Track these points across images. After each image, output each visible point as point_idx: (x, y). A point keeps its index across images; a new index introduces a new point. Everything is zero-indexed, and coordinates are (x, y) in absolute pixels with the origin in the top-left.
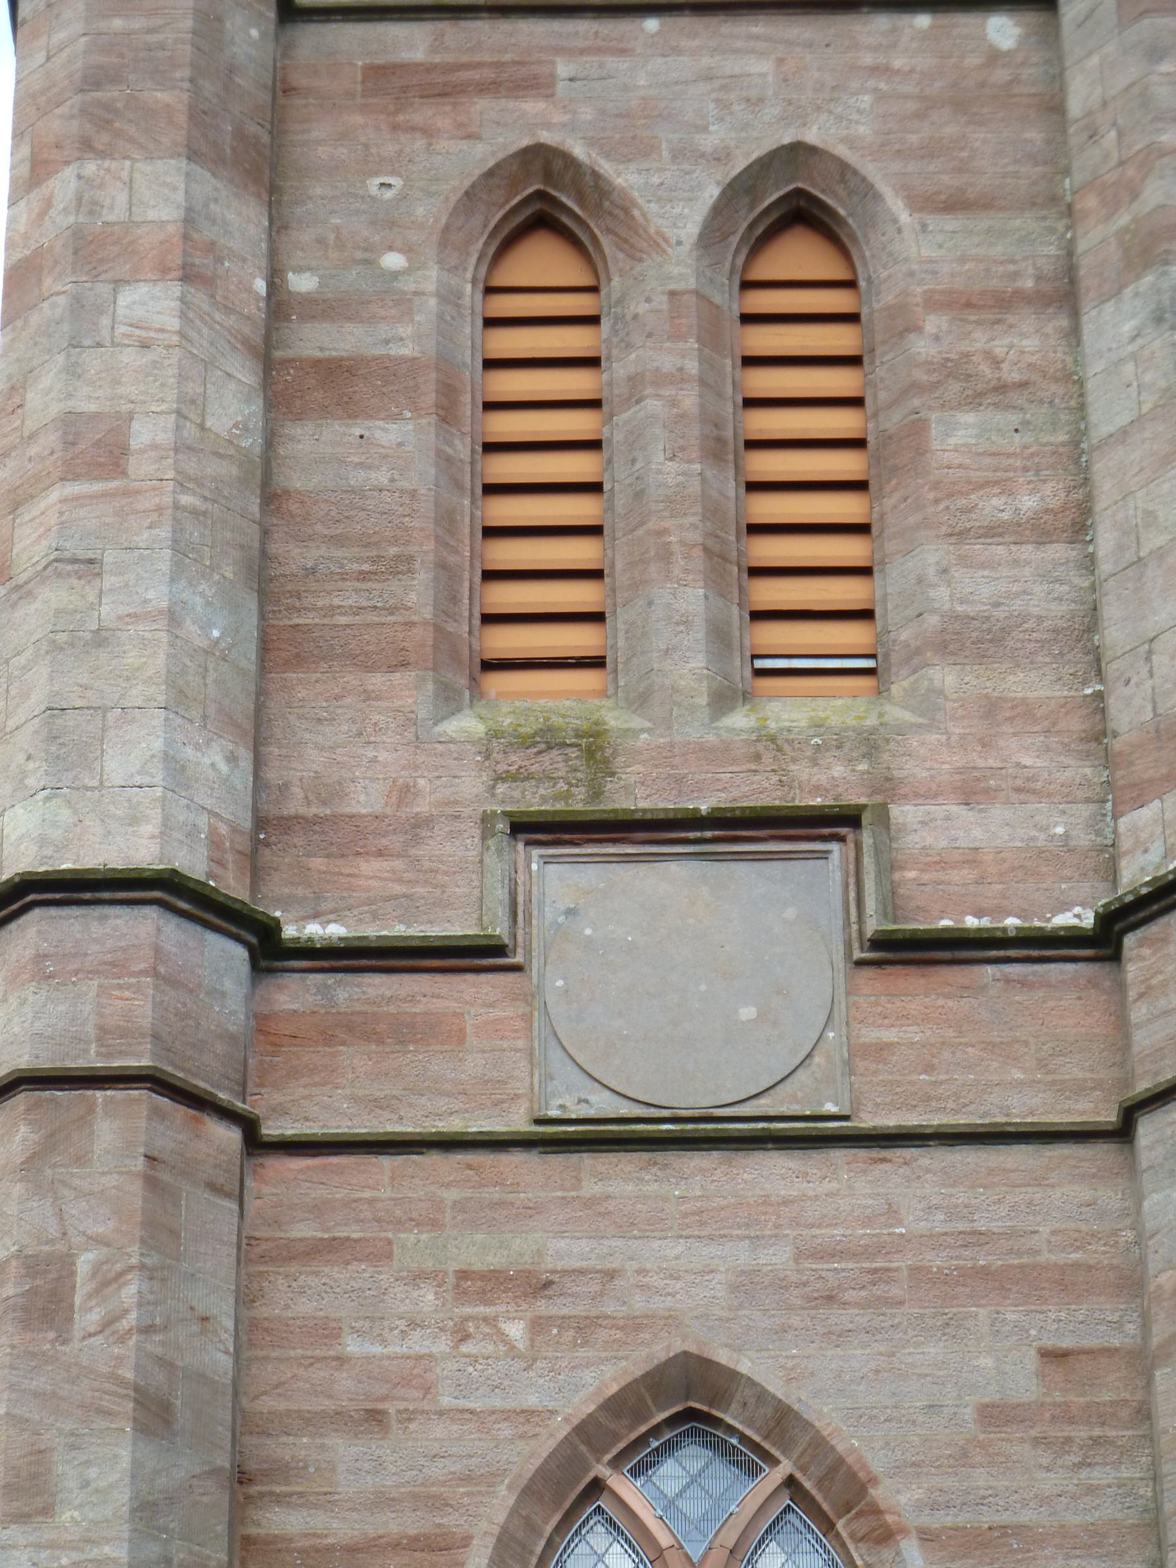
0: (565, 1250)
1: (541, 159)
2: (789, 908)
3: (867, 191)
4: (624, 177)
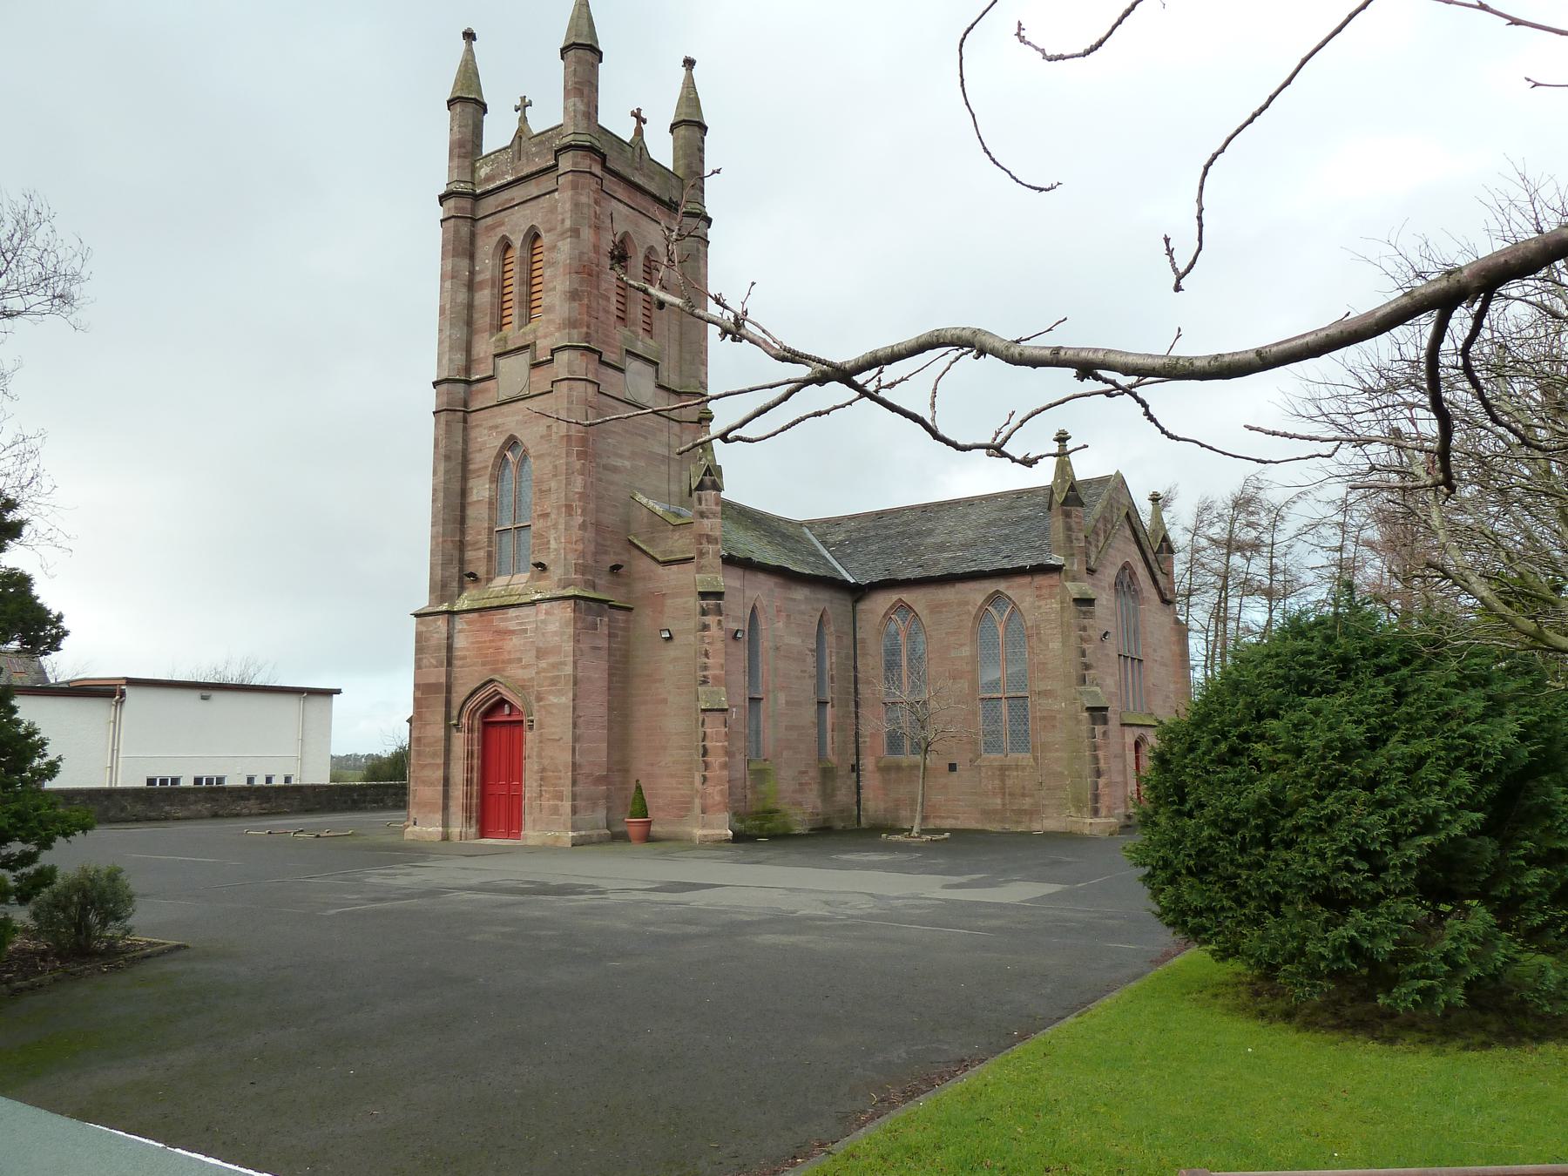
0: (500, 421)
2: (524, 359)
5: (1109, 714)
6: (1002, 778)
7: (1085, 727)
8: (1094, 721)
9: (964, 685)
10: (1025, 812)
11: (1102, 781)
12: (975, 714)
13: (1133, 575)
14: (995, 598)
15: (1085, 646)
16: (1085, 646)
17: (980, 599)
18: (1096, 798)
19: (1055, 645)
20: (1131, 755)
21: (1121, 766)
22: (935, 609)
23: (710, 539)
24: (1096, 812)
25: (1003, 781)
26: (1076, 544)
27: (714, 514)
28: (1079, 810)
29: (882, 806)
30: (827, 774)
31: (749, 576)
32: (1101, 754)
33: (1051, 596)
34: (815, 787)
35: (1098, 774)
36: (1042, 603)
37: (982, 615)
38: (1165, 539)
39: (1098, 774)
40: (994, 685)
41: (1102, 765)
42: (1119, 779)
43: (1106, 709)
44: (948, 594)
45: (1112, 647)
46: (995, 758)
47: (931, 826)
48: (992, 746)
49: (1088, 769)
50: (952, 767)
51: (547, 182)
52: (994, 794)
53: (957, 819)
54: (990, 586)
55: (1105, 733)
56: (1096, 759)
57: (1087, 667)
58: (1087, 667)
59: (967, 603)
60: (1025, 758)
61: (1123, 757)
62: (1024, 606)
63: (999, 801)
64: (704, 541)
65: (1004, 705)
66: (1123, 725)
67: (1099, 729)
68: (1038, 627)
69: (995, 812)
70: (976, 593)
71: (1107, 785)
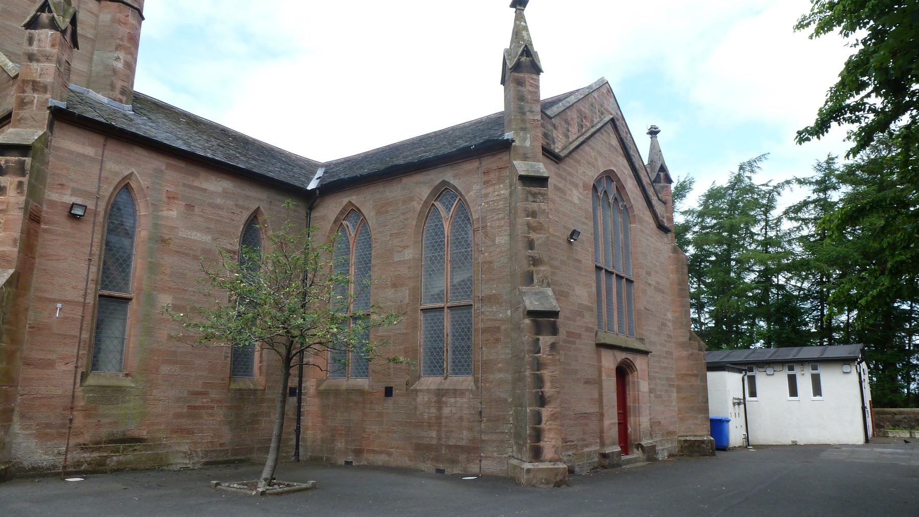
5: (560, 320)
6: (440, 405)
7: (527, 338)
8: (538, 329)
9: (404, 294)
10: (463, 449)
11: (546, 412)
12: (415, 327)
13: (621, 188)
14: (443, 191)
15: (533, 235)
16: (533, 235)
17: (425, 192)
18: (538, 435)
19: (502, 239)
20: (610, 384)
21: (596, 395)
22: (381, 210)
23: (36, 86)
24: (537, 454)
25: (440, 409)
26: (529, 116)
27: (48, 58)
28: (520, 448)
29: (319, 436)
30: (243, 401)
31: (112, 146)
32: (546, 373)
33: (500, 180)
34: (220, 413)
35: (542, 401)
36: (490, 189)
37: (429, 210)
38: (663, 169)
39: (542, 401)
40: (440, 296)
41: (548, 389)
42: (593, 409)
43: (555, 314)
44: (394, 191)
45: (585, 254)
46: (430, 382)
47: (364, 463)
48: (436, 368)
49: (528, 392)
50: (389, 392)
52: (430, 425)
53: (389, 454)
54: (435, 177)
55: (553, 346)
56: (539, 381)
57: (536, 262)
58: (536, 262)
59: (411, 199)
60: (465, 382)
61: (598, 382)
62: (470, 196)
63: (434, 434)
64: (29, 89)
65: (447, 316)
66: (600, 346)
67: (545, 340)
68: (484, 219)
69: (428, 448)
70: (420, 188)
71: (554, 417)
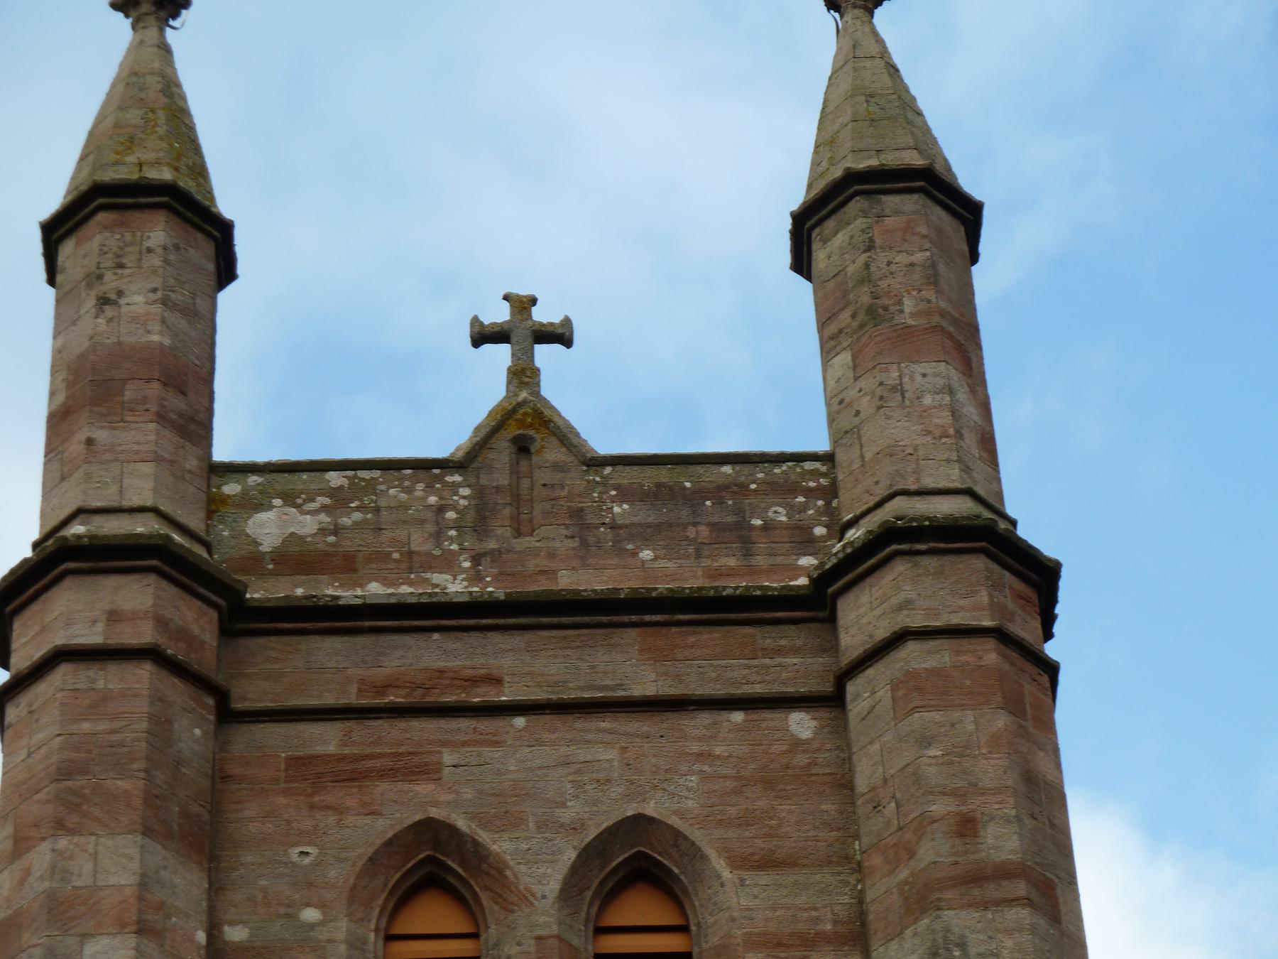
1: (432, 832)
3: (696, 854)
4: (499, 845)
51: (789, 661)
